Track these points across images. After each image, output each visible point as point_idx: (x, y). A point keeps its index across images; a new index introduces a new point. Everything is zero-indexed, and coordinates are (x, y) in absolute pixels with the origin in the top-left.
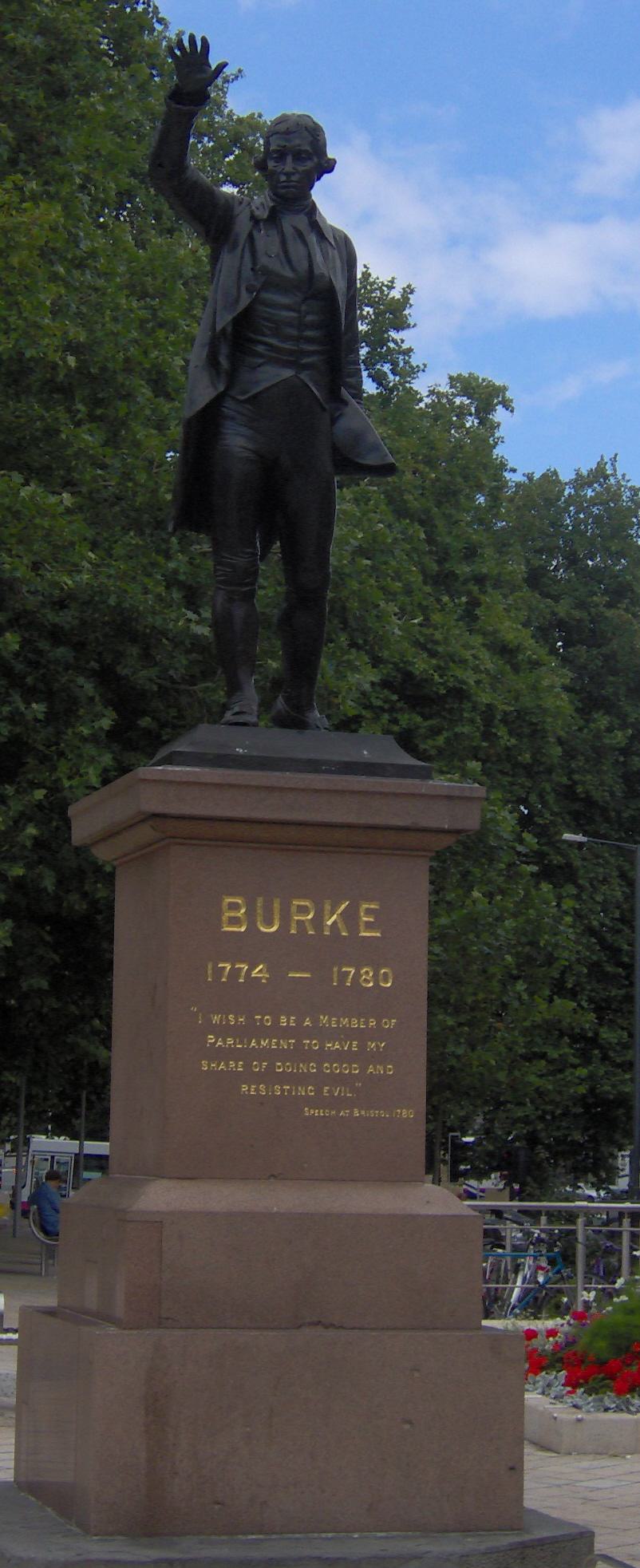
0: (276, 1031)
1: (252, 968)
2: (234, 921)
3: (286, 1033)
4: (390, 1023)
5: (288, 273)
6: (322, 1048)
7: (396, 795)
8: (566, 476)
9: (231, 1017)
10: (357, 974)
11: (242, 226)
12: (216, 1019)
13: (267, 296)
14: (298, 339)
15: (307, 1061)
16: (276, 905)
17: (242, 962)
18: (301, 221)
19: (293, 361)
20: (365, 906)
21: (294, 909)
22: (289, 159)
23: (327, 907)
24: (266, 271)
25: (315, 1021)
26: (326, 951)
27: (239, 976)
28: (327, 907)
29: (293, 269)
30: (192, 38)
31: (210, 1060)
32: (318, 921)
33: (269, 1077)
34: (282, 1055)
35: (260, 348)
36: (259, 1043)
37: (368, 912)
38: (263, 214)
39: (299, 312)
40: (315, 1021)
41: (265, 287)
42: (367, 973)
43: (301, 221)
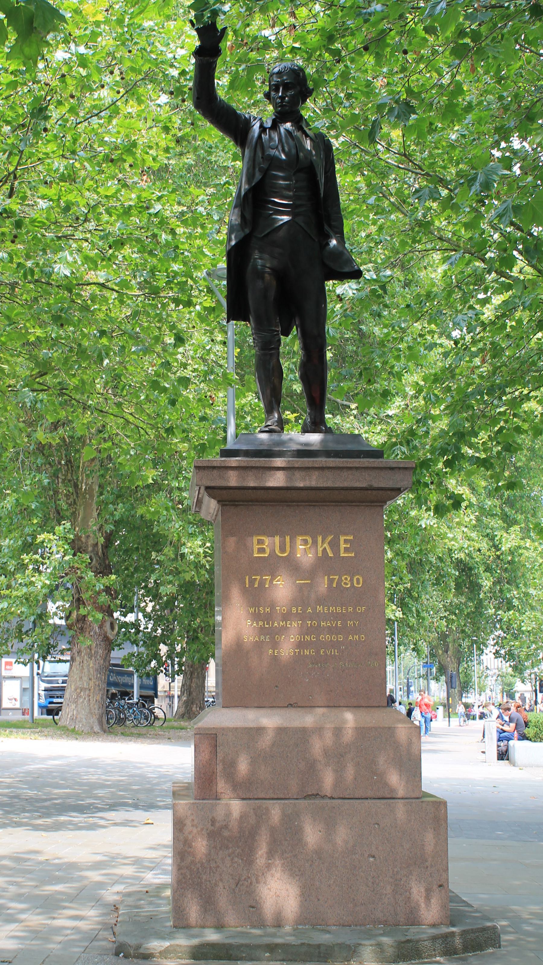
6: (319, 625)
10: (340, 580)
27: (265, 584)
28: (320, 539)
38: (269, 124)
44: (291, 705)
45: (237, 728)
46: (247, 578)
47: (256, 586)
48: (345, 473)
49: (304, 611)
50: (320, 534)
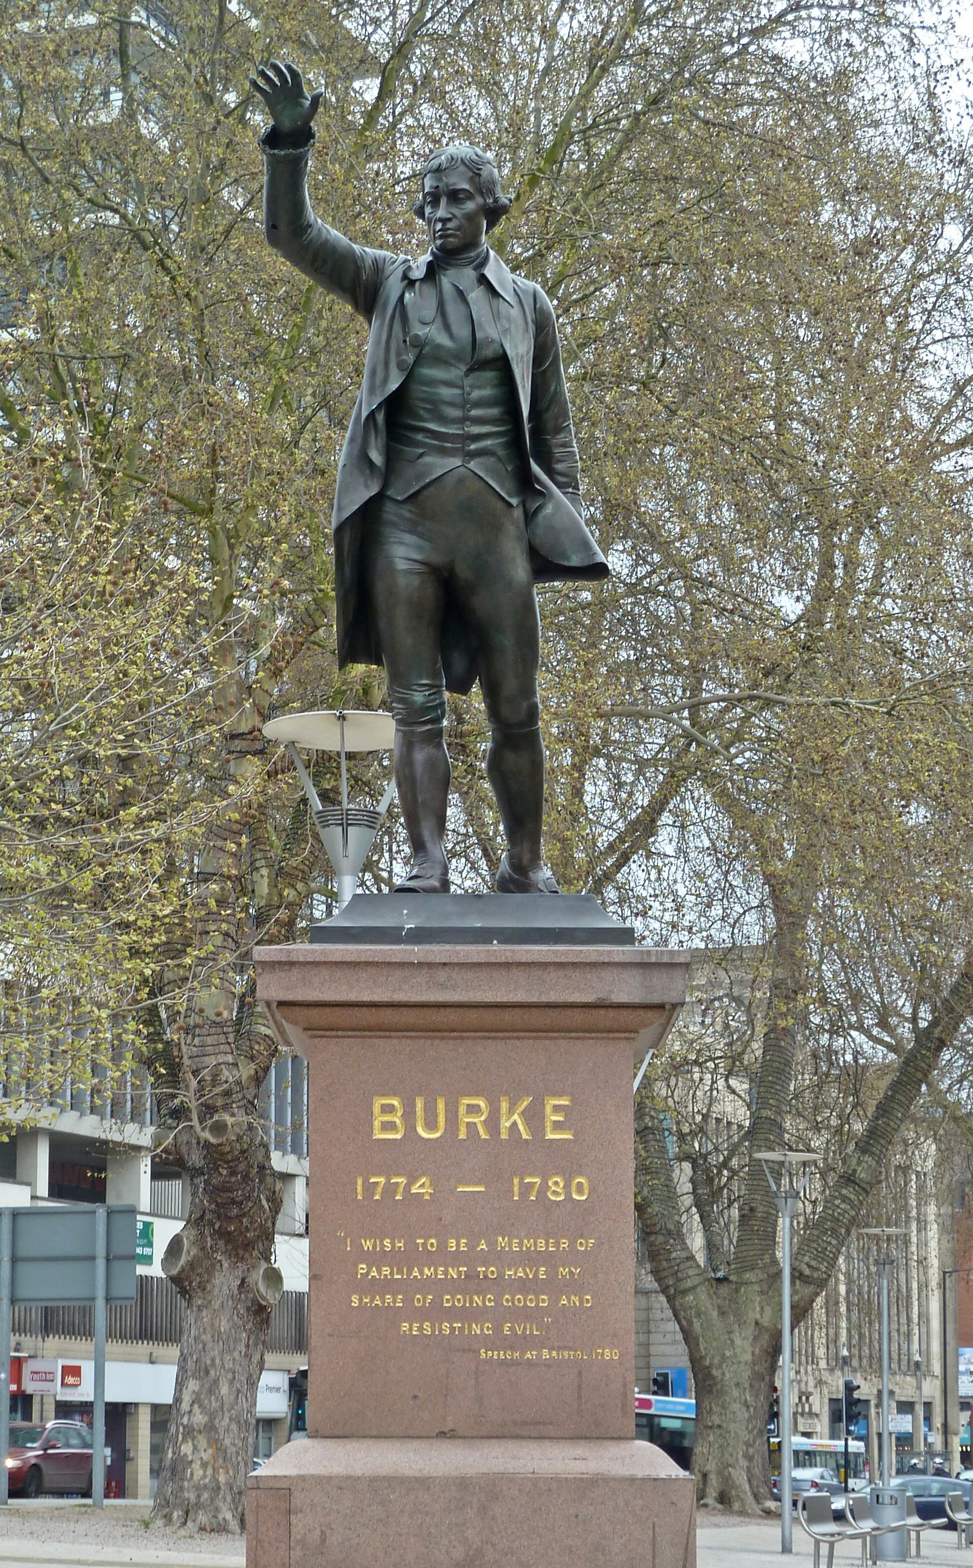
0: (442, 1257)
1: (412, 1180)
2: (389, 1126)
3: (456, 1258)
4: (585, 1245)
5: (443, 340)
6: (501, 1275)
7: (575, 965)
9: (387, 1242)
10: (544, 1187)
11: (393, 286)
12: (368, 1245)
14: (462, 421)
15: (481, 1292)
16: (441, 1106)
17: (399, 1175)
19: (462, 446)
20: (466, 1101)
21: (462, 1110)
22: (443, 201)
23: (504, 1106)
24: (419, 344)
25: (492, 1243)
26: (503, 1158)
27: (395, 1193)
28: (504, 1106)
29: (451, 336)
31: (362, 1293)
32: (493, 1123)
33: (436, 1313)
34: (454, 1287)
35: (420, 437)
36: (421, 1273)
37: (557, 1109)
38: (418, 272)
39: (462, 388)
40: (492, 1243)
42: (556, 1184)
44: (442, 1435)
45: (330, 1478)
46: (360, 1182)
47: (377, 1197)
48: (552, 976)
49: (472, 1246)
50: (506, 1093)
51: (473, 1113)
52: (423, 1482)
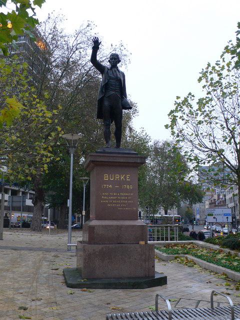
3: (115, 196)
8: (230, 54)
13: (110, 80)
14: (115, 87)
18: (116, 69)
19: (115, 90)
24: (110, 77)
26: (120, 183)
30: (96, 38)
41: (110, 79)
43: (116, 69)
51: (117, 177)
52: (112, 226)
